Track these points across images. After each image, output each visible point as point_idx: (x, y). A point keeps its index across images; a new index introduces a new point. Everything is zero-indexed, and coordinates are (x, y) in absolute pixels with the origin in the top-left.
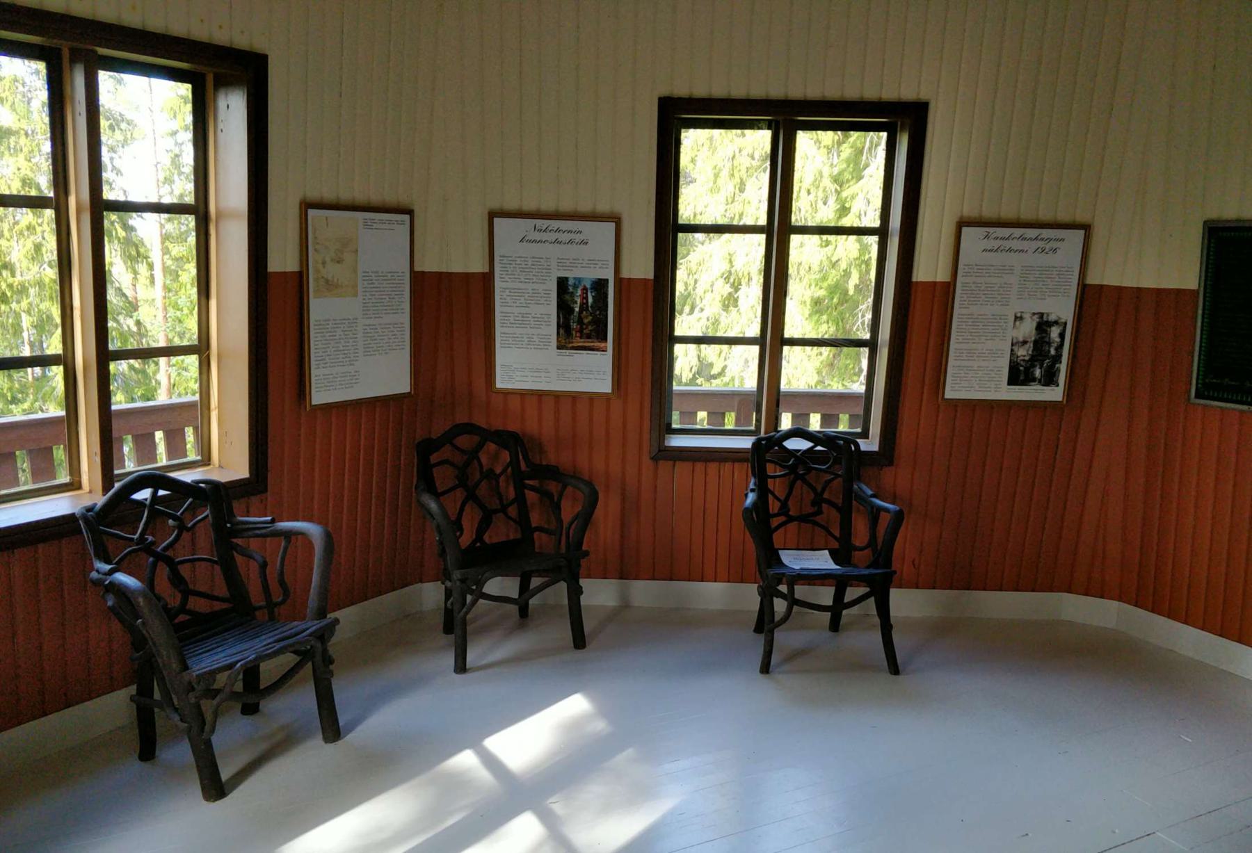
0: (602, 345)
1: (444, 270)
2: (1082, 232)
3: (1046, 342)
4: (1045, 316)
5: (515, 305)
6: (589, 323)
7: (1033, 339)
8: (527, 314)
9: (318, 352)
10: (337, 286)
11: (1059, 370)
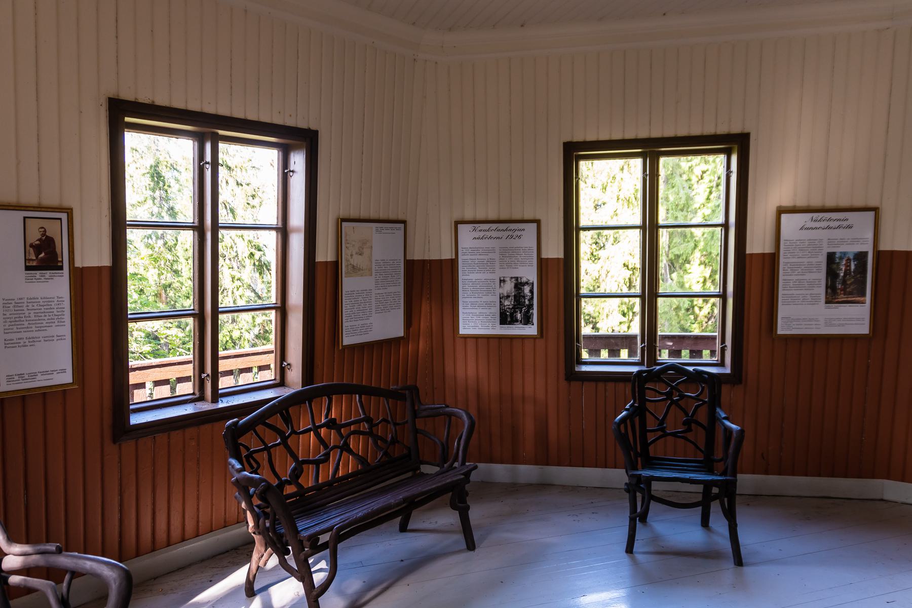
0: (862, 299)
1: (751, 253)
2: (874, 212)
3: (522, 296)
4: (519, 279)
5: (794, 274)
6: (851, 284)
7: (513, 294)
8: (803, 280)
9: (347, 312)
10: (359, 270)
11: (532, 314)
